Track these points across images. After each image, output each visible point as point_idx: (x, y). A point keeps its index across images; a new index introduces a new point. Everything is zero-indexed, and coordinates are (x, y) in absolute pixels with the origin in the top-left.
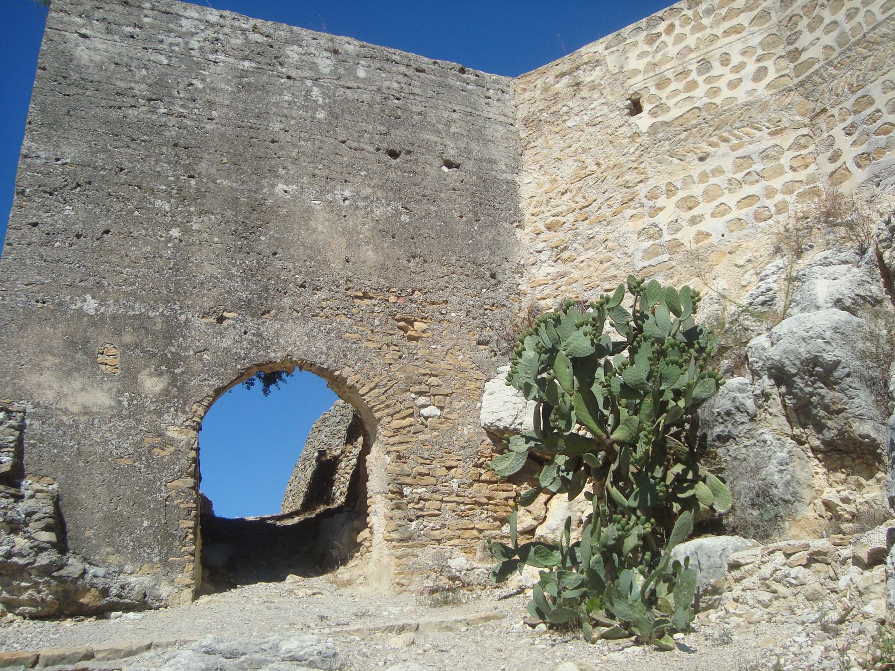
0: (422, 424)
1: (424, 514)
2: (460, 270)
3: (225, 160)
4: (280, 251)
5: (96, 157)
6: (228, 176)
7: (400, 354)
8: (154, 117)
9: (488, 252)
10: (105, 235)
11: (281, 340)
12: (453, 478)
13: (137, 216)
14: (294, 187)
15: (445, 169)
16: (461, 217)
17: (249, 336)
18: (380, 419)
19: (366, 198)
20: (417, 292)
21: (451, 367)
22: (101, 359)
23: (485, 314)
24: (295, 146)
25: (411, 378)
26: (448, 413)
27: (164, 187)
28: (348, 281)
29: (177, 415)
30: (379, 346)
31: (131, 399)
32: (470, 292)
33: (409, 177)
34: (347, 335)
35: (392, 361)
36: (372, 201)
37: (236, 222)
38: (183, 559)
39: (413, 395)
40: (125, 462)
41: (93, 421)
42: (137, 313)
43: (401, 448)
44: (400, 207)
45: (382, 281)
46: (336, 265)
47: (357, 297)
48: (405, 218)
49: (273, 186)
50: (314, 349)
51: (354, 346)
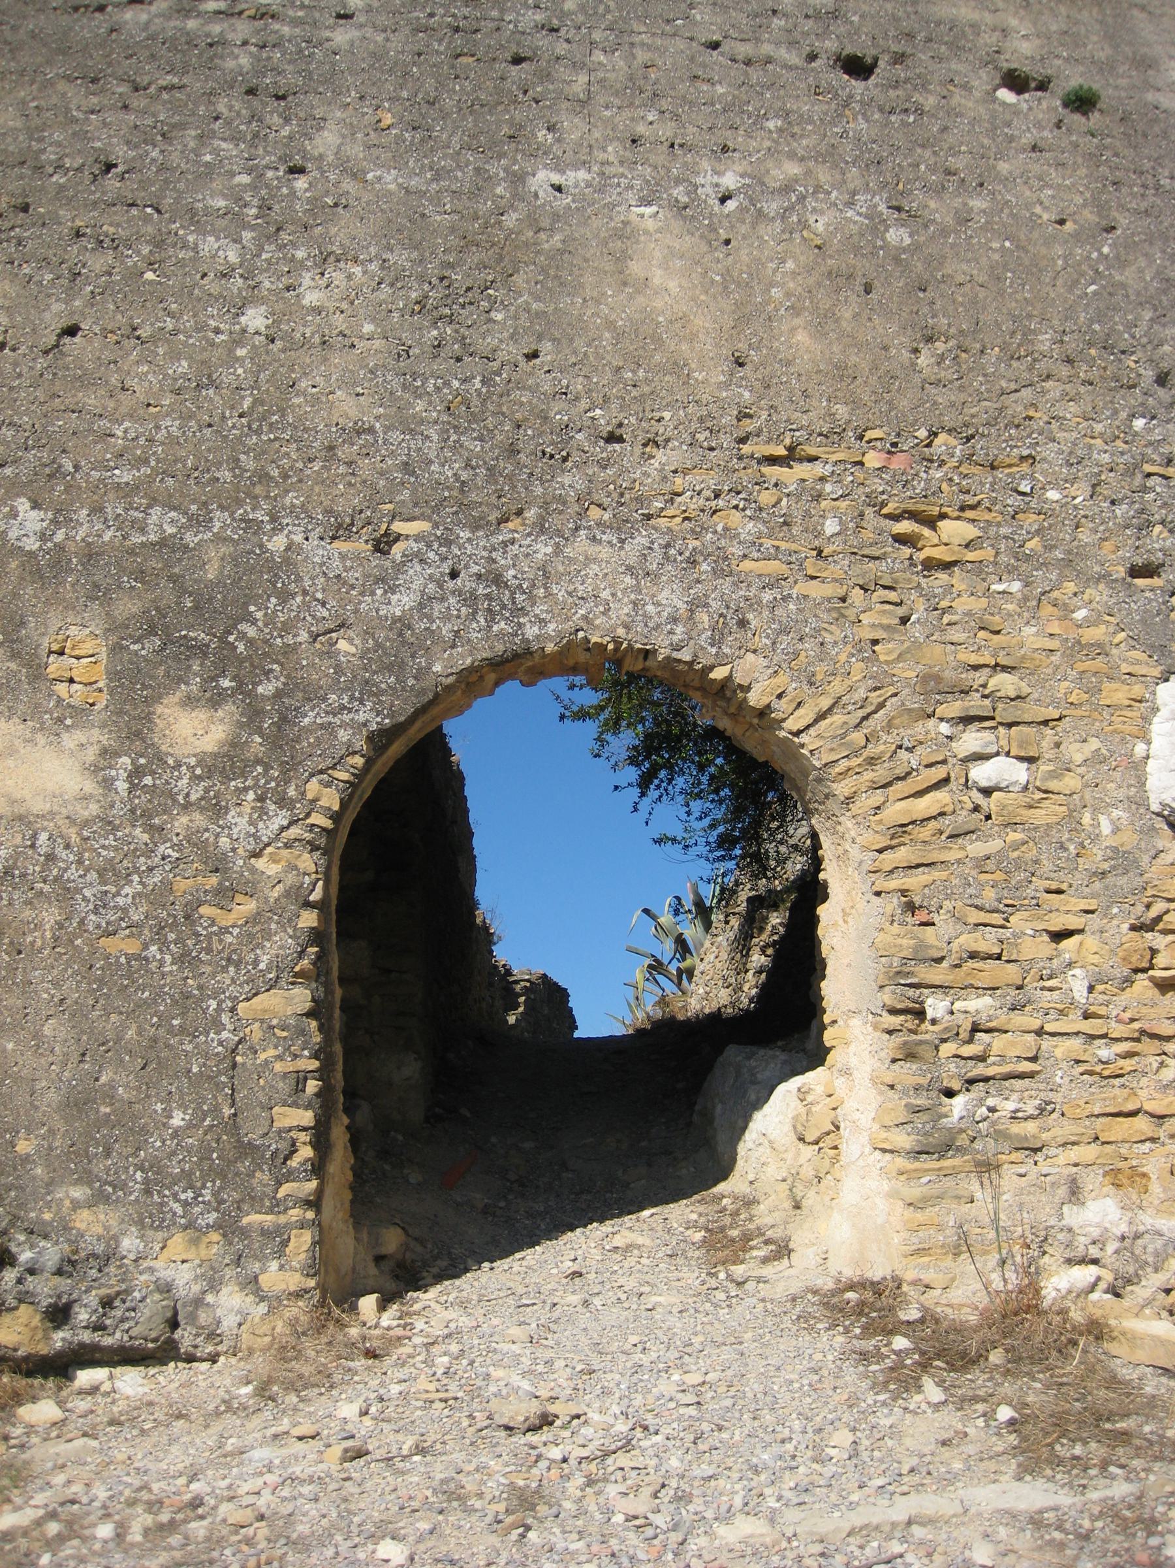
0: (976, 809)
1: (990, 1072)
2: (1065, 371)
3: (388, 119)
4: (546, 347)
5: (41, 140)
6: (398, 162)
7: (901, 611)
8: (191, 24)
9: (1148, 315)
10: (67, 340)
11: (555, 589)
12: (1070, 965)
13: (151, 282)
14: (582, 175)
15: (1005, 95)
16: (1062, 222)
17: (464, 582)
18: (849, 800)
19: (787, 189)
20: (942, 437)
21: (1054, 644)
22: (55, 666)
23: (1145, 489)
24: (577, 66)
25: (938, 678)
26: (1053, 775)
27: (221, 203)
28: (742, 416)
29: (263, 812)
30: (841, 592)
31: (136, 773)
32: (1099, 428)
33: (904, 124)
34: (747, 565)
35: (879, 634)
36: (802, 198)
37: (422, 278)
38: (282, 1219)
39: (945, 728)
40: (122, 945)
41: (34, 836)
42: (153, 537)
43: (915, 881)
44: (882, 207)
45: (841, 410)
46: (710, 376)
47: (772, 460)
48: (897, 236)
49: (518, 179)
50: (650, 608)
51: (767, 596)
